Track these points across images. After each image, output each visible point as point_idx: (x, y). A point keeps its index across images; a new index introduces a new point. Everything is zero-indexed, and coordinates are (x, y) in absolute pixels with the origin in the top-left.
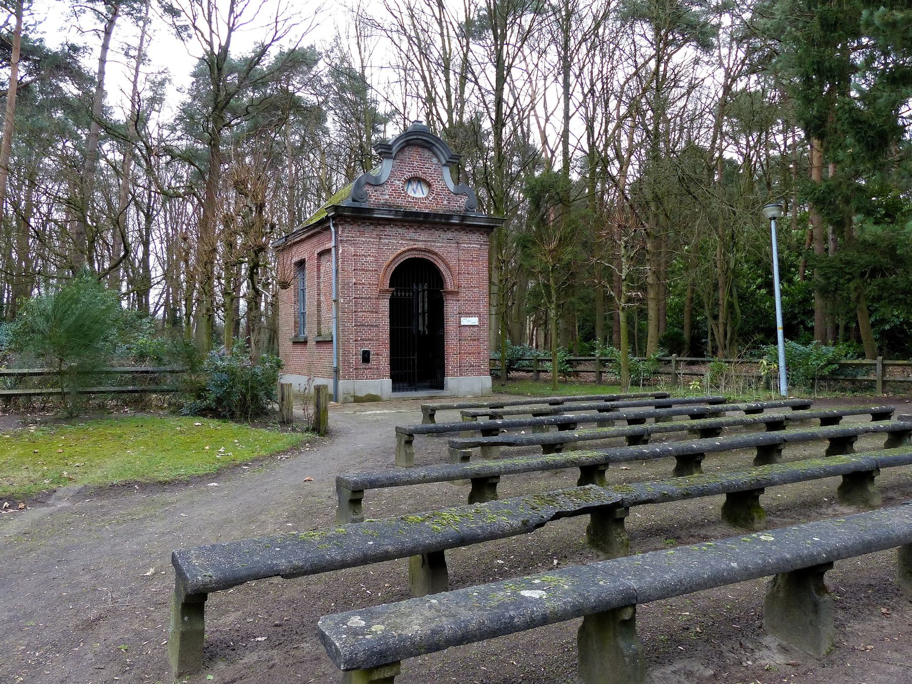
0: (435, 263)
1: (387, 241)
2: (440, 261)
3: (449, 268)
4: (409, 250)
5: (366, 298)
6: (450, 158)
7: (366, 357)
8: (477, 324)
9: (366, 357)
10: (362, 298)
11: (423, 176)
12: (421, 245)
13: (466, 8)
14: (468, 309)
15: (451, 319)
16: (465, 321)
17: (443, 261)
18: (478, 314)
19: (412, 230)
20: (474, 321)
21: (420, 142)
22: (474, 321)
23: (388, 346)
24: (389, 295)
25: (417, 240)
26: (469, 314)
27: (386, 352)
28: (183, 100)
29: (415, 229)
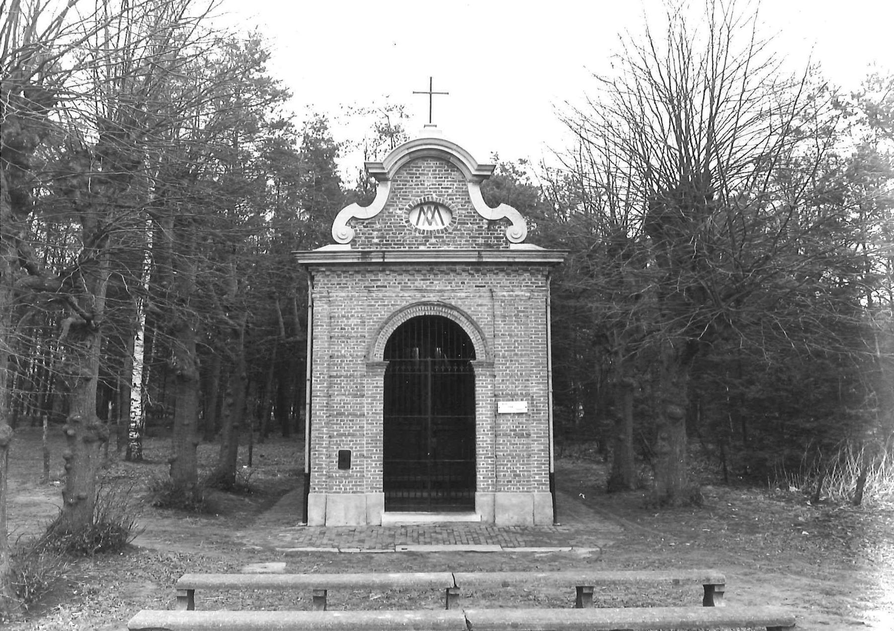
0: (457, 321)
1: (380, 295)
2: (463, 318)
3: (480, 332)
4: (412, 306)
5: (346, 377)
6: (477, 170)
7: (344, 460)
8: (526, 411)
9: (344, 460)
10: (340, 377)
11: (440, 200)
12: (433, 298)
13: (51, 26)
14: (510, 388)
15: (317, 368)
16: (504, 407)
17: (468, 318)
18: (526, 396)
19: (418, 277)
20: (521, 406)
21: (433, 153)
22: (521, 406)
23: (381, 445)
24: (382, 371)
25: (426, 291)
26: (513, 397)
27: (378, 455)
28: (336, 133)
29: (425, 275)
